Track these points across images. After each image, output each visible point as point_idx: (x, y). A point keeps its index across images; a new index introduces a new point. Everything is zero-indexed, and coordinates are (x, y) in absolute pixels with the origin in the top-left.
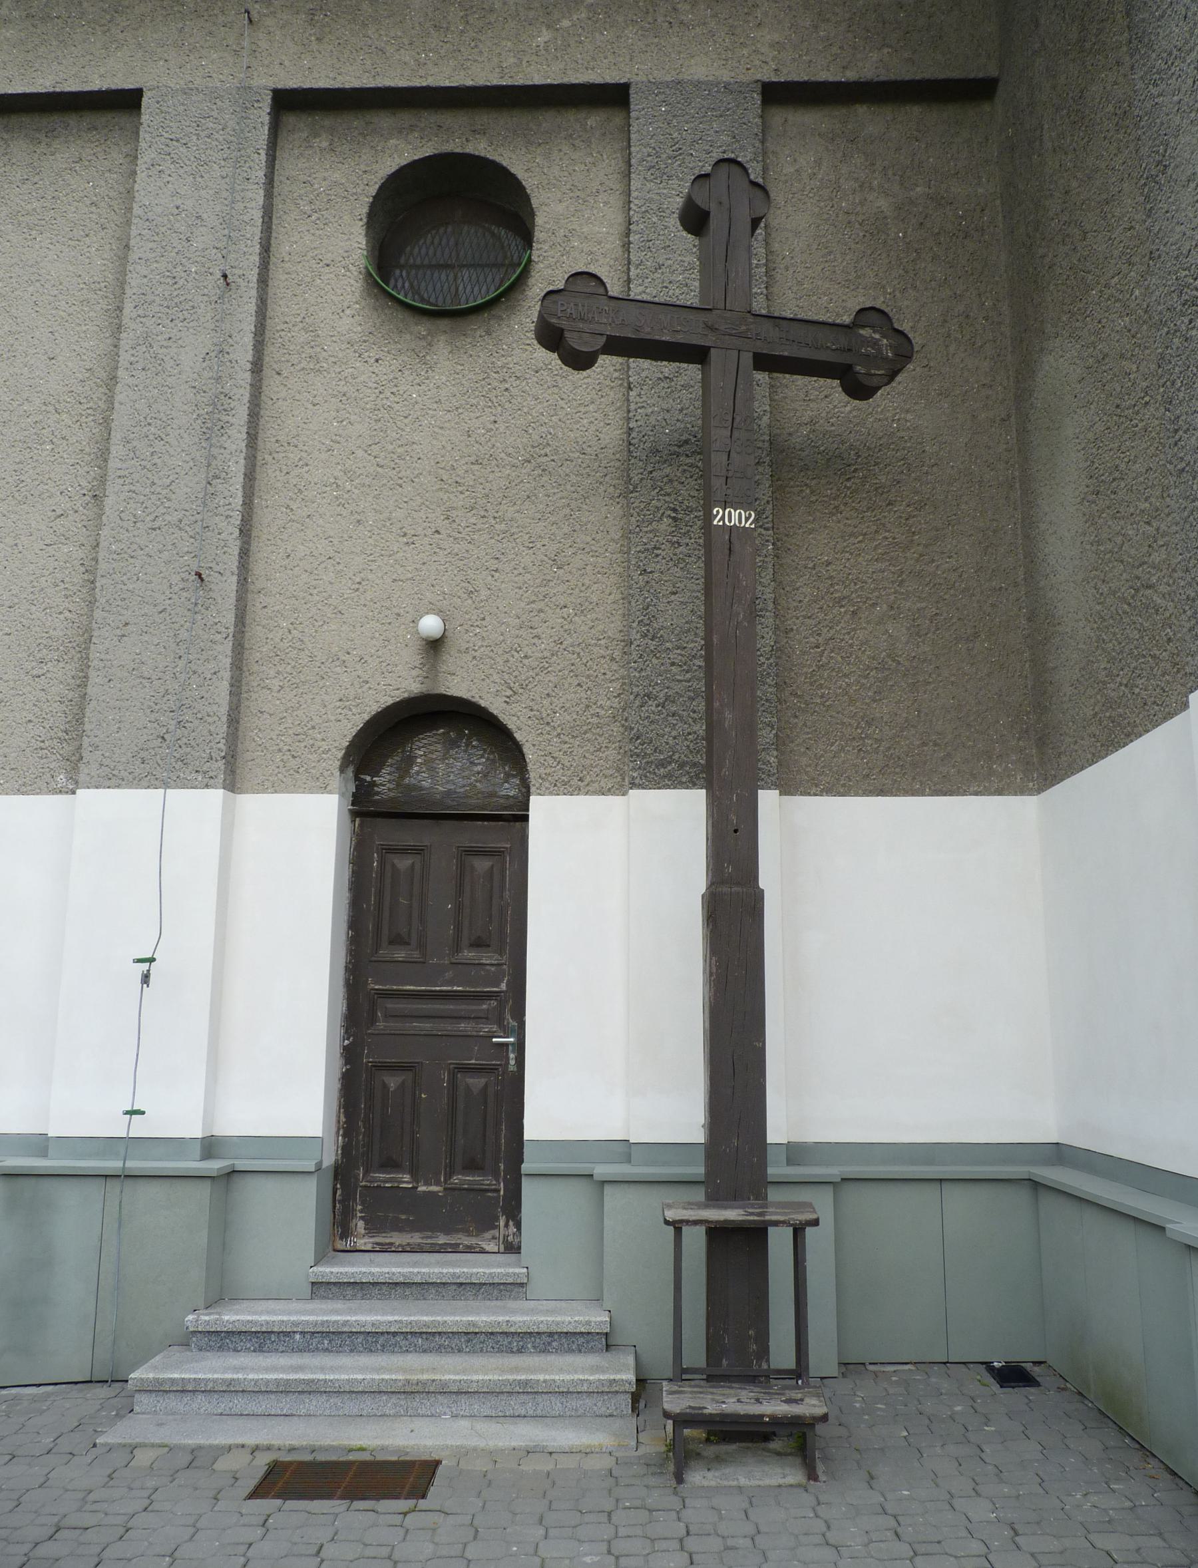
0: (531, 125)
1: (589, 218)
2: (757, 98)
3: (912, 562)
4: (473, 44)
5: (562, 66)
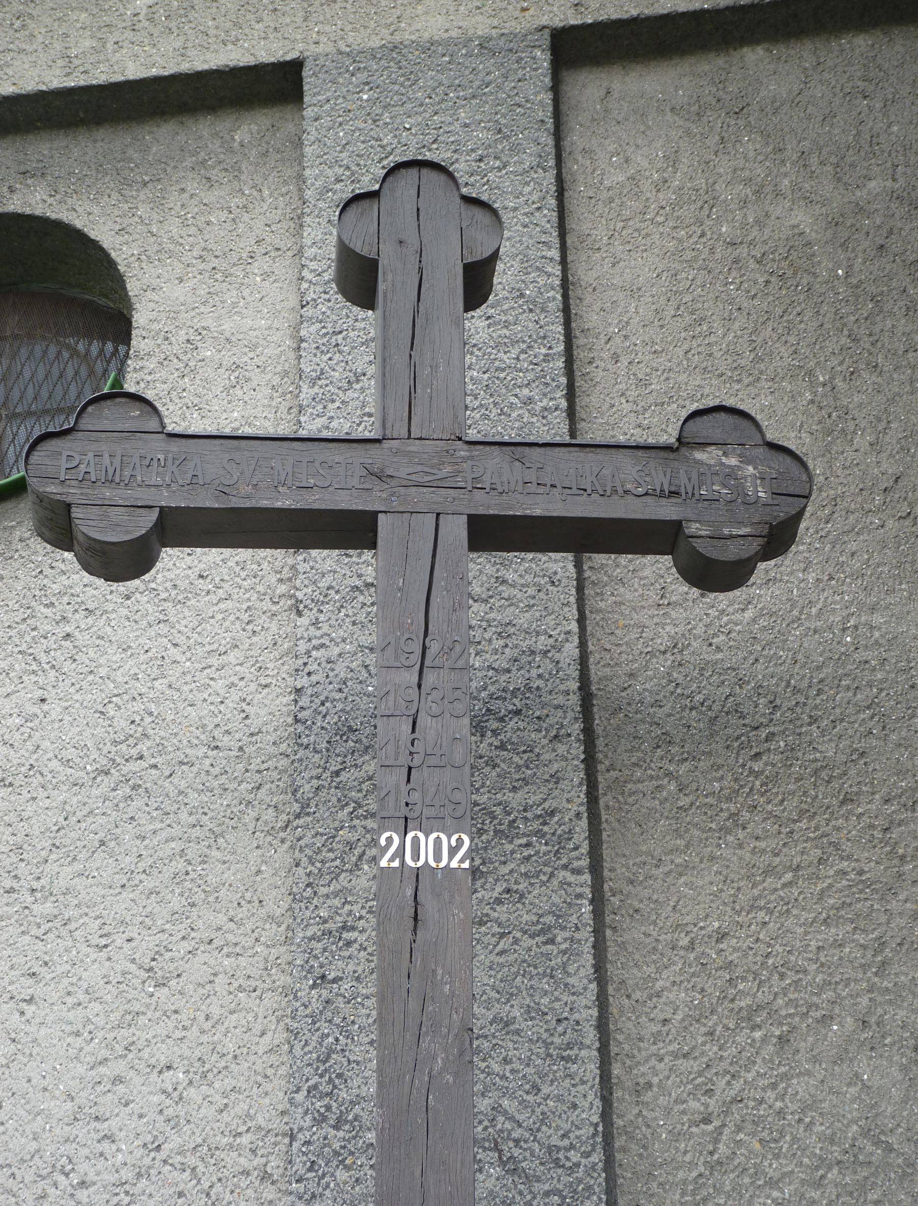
0: (130, 152)
1: (234, 305)
2: (543, 58)
3: (903, 922)
4: (18, 24)
5: (178, 44)
